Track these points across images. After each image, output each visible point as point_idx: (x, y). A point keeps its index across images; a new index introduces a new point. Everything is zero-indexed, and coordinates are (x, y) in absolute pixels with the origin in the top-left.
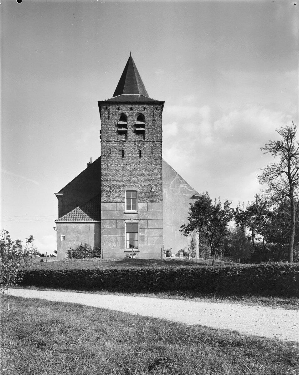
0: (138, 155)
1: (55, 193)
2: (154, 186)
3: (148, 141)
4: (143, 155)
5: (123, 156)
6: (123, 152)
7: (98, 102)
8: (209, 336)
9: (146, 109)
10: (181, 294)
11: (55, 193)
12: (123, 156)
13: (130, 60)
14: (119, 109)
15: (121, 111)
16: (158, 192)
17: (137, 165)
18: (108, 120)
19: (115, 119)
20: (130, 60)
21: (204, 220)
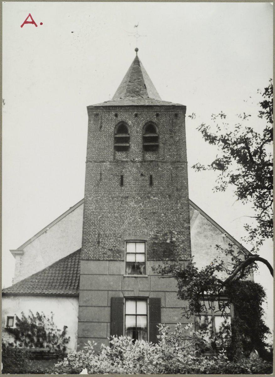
0: (148, 183)
1: (11, 251)
2: (176, 233)
3: (165, 161)
4: (155, 183)
5: (122, 184)
6: (122, 177)
7: (87, 107)
8: (203, 359)
9: (160, 115)
10: (130, 301)
11: (11, 251)
12: (122, 184)
13: (137, 62)
14: (116, 115)
15: (119, 119)
16: (183, 242)
17: (145, 198)
18: (100, 131)
19: (110, 128)
20: (137, 62)
21: (263, 178)
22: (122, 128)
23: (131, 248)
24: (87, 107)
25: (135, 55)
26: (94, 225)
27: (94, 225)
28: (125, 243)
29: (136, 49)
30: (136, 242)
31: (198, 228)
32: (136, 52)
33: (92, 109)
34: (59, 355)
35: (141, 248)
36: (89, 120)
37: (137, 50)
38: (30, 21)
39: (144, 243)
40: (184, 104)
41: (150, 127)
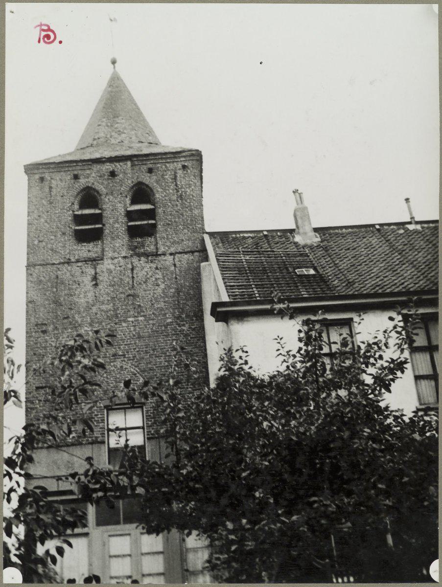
15: (83, 182)
22: (89, 198)
23: (116, 420)
24: (25, 166)
25: (112, 70)
26: (122, 347)
27: (122, 347)
28: (105, 411)
29: (112, 60)
30: (125, 409)
31: (143, 428)
32: (112, 66)
33: (31, 169)
34: (371, 411)
35: (135, 418)
36: (30, 187)
37: (114, 62)
38: (48, 36)
39: (348, 326)
40: (194, 147)
41: (141, 193)
